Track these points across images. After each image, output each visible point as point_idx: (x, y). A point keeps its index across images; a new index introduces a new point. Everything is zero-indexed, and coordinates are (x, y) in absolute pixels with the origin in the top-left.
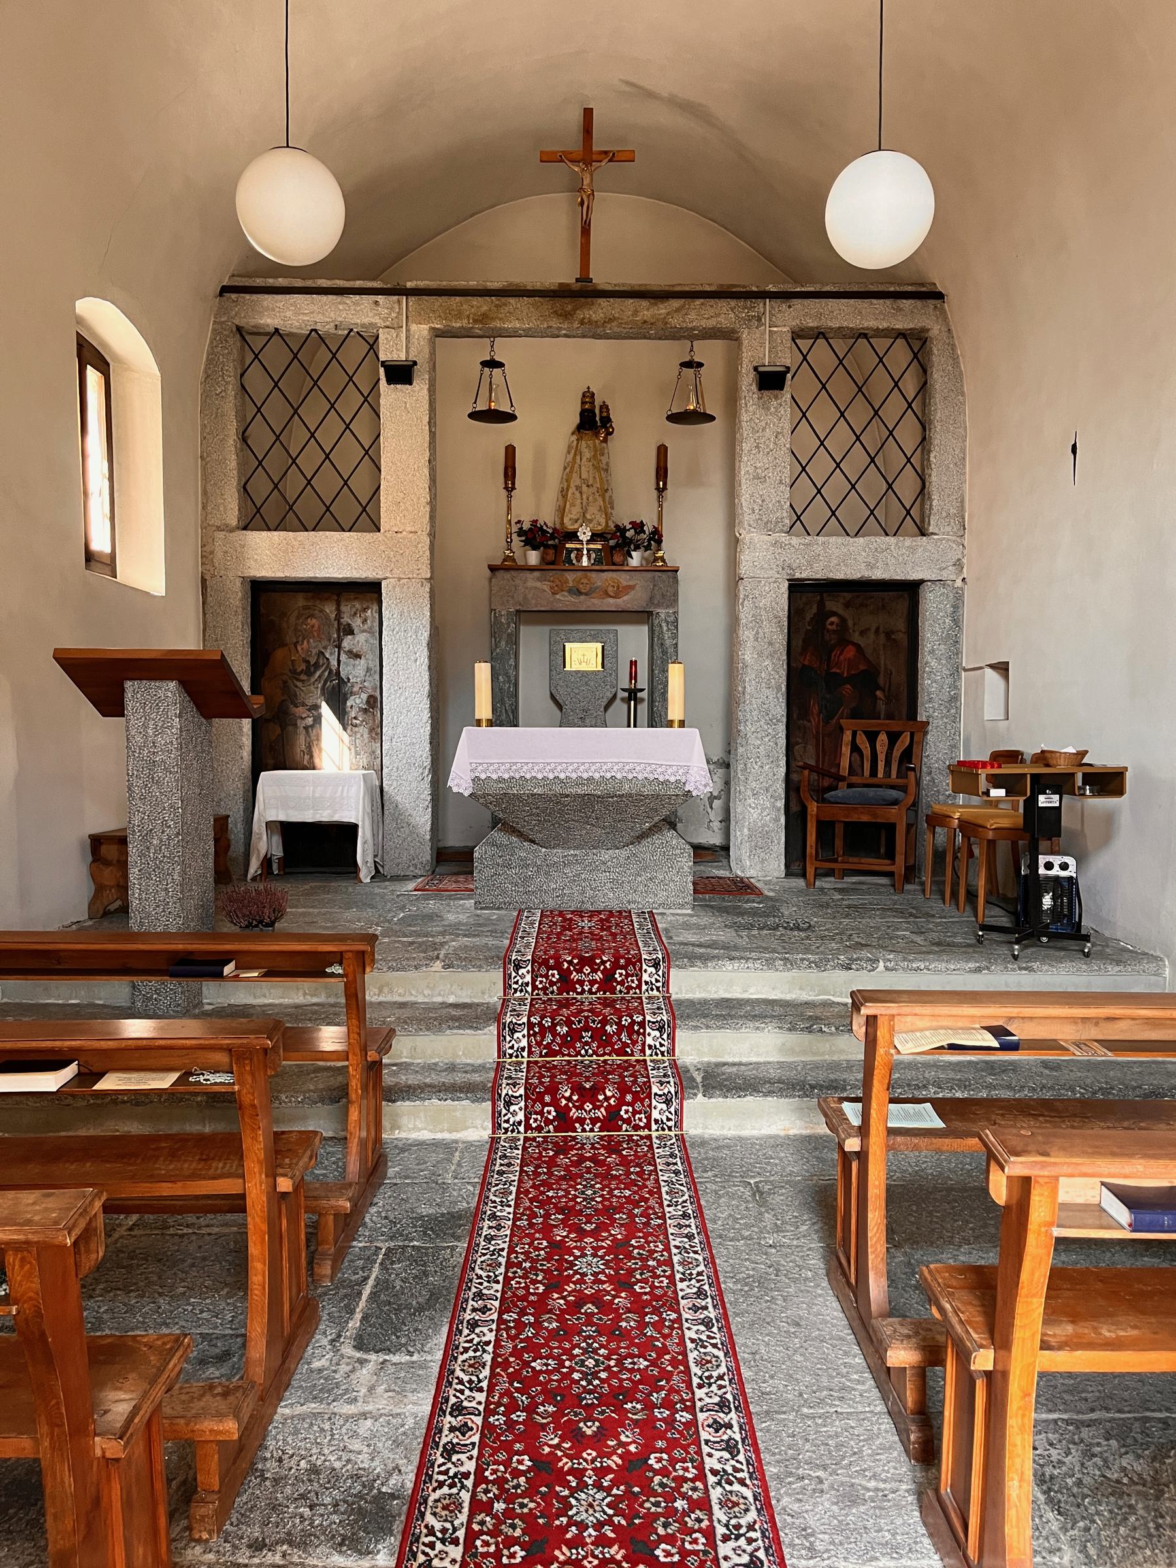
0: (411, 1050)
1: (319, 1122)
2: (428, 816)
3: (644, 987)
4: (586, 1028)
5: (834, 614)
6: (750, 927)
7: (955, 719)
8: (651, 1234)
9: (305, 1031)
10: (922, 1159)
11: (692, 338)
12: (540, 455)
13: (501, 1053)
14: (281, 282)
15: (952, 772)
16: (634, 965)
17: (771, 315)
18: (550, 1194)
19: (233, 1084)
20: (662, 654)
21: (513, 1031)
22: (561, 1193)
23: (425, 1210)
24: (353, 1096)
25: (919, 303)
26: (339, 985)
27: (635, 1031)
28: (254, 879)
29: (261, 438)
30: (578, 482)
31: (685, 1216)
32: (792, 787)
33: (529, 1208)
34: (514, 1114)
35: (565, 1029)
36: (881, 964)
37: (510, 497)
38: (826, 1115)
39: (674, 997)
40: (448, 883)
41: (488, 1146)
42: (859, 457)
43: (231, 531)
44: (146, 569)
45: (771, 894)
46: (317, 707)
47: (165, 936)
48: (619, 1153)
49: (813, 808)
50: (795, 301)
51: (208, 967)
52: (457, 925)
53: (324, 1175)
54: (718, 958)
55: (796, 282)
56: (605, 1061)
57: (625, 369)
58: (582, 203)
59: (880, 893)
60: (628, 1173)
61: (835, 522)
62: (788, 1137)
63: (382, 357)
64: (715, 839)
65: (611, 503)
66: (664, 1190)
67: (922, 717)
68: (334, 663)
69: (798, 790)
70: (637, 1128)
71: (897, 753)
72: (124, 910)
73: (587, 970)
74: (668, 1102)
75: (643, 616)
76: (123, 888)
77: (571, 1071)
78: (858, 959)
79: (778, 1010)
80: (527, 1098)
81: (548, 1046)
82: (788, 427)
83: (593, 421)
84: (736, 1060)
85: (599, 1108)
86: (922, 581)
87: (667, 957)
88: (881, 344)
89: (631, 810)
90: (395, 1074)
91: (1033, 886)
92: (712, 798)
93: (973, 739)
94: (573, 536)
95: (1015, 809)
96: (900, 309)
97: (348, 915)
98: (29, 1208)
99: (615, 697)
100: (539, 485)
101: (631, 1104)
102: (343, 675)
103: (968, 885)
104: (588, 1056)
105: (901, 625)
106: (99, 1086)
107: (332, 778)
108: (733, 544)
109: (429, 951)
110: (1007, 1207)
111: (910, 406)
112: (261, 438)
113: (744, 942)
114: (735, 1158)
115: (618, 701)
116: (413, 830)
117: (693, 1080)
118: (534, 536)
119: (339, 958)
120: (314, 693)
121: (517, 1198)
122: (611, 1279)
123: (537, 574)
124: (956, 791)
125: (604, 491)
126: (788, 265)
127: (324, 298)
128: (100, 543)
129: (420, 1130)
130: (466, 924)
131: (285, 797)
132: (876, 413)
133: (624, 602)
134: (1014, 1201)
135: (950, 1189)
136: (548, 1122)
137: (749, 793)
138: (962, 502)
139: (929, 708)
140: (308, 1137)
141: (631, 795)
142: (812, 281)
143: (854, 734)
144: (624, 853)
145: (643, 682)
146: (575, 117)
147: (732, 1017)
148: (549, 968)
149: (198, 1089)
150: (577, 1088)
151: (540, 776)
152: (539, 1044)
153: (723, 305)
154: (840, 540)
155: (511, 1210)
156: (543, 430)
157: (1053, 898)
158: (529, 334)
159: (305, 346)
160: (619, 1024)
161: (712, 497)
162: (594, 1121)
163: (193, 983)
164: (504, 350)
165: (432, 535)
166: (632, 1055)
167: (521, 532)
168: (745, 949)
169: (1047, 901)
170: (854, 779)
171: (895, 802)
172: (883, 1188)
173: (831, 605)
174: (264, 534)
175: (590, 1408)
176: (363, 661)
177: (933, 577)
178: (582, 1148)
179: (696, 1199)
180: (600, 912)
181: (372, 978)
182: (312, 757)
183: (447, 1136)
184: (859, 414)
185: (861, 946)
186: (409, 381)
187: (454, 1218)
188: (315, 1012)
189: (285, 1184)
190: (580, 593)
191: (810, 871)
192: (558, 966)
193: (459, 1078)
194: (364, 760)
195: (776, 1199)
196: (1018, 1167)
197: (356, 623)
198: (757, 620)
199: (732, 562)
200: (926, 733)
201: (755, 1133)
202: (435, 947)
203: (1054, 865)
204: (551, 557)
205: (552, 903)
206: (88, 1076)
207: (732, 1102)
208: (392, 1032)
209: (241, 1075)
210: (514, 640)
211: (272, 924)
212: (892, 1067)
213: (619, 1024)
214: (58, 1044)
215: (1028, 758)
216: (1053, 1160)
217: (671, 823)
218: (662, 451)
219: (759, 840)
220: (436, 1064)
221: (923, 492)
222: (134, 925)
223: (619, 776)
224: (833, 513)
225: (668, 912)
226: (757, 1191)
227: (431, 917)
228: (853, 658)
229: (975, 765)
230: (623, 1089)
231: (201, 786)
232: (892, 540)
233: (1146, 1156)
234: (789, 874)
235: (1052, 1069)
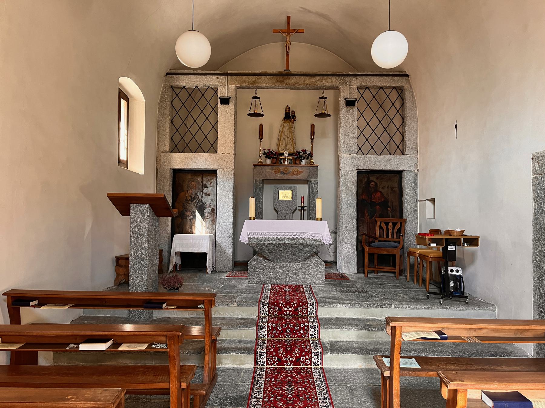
0: (228, 335)
1: (192, 362)
2: (231, 250)
3: (308, 313)
4: (288, 328)
5: (373, 181)
6: (346, 291)
7: (416, 218)
8: (313, 405)
9: (189, 328)
10: (411, 379)
11: (323, 89)
12: (271, 127)
13: (258, 336)
14: (186, 71)
15: (417, 237)
16: (305, 305)
17: (350, 82)
18: (276, 389)
20: (313, 195)
21: (262, 329)
22: (280, 389)
23: (231, 394)
24: (207, 352)
25: (400, 78)
26: (202, 312)
27: (306, 329)
28: (171, 272)
29: (178, 122)
30: (284, 137)
31: (325, 398)
32: (359, 241)
33: (269, 394)
34: (263, 359)
35: (281, 328)
36: (393, 306)
37: (261, 141)
38: (376, 362)
42: (380, 129)
43: (167, 153)
44: (138, 165)
47: (141, 293)
48: (300, 374)
49: (367, 249)
50: (358, 77)
51: (157, 305)
53: (195, 381)
54: (335, 303)
55: (358, 71)
56: (295, 340)
57: (302, 100)
58: (287, 46)
60: (304, 382)
61: (373, 150)
63: (219, 96)
64: (331, 259)
65: (295, 144)
66: (317, 388)
67: (404, 217)
69: (361, 242)
70: (306, 365)
71: (396, 230)
72: (127, 283)
73: (288, 307)
74: (318, 356)
75: (306, 181)
76: (127, 275)
77: (283, 344)
78: (385, 304)
79: (357, 322)
80: (267, 353)
81: (274, 334)
82: (356, 119)
83: (289, 116)
84: (342, 340)
85: (293, 357)
86: (403, 171)
87: (317, 302)
88: (388, 91)
89: (303, 249)
90: (220, 343)
91: (446, 278)
92: (330, 244)
93: (423, 226)
94: (282, 154)
95: (439, 249)
96: (394, 80)
97: (204, 285)
98: (100, 395)
99: (296, 209)
100: (271, 137)
101: (304, 356)
102: (203, 201)
103: (422, 277)
104: (289, 338)
105: (396, 185)
107: (199, 236)
109: (232, 299)
110: (448, 400)
111: (398, 111)
112: (178, 122)
113: (344, 297)
114: (342, 376)
115: (297, 211)
116: (226, 254)
117: (327, 347)
118: (269, 154)
119: (203, 302)
121: (264, 390)
123: (270, 167)
124: (418, 244)
125: (293, 140)
126: (354, 64)
127: (200, 76)
128: (123, 157)
129: (229, 364)
130: (245, 289)
131: (183, 243)
132: (386, 114)
133: (300, 177)
134: (451, 398)
135: (421, 390)
136: (275, 362)
137: (344, 243)
138: (417, 143)
140: (191, 368)
141: (303, 244)
142: (364, 71)
143: (381, 223)
144: (301, 264)
145: (306, 204)
146: (285, 19)
147: (340, 324)
148: (275, 306)
149: (155, 350)
151: (271, 237)
152: (271, 333)
153: (334, 78)
154: (375, 156)
155: (262, 395)
156: (273, 120)
157: (454, 283)
158: (268, 88)
159: (192, 92)
160: (300, 326)
161: (329, 142)
162: (291, 362)
163: (150, 310)
165: (235, 154)
167: (264, 153)
168: (344, 300)
169: (452, 283)
170: (381, 239)
171: (396, 247)
172: (399, 390)
173: (372, 178)
174: (178, 154)
176: (210, 197)
178: (287, 372)
179: (328, 392)
180: (292, 285)
182: (192, 229)
183: (238, 366)
184: (380, 114)
187: (242, 397)
188: (192, 321)
189: (184, 385)
190: (285, 174)
191: (366, 271)
192: (278, 305)
193: (243, 345)
196: (452, 386)
197: (208, 184)
198: (346, 184)
199: (337, 163)
200: (406, 223)
201: (349, 367)
202: (235, 297)
203: (454, 271)
204: (274, 161)
205: (275, 282)
206: (116, 345)
207: (341, 356)
208: (220, 329)
209: (170, 345)
210: (262, 190)
211: (178, 289)
213: (300, 326)
214: (107, 333)
217: (316, 254)
218: (313, 126)
219: (348, 261)
220: (234, 340)
221: (403, 140)
222: (131, 289)
223: (299, 237)
224: (372, 147)
225: (316, 285)
226: (351, 389)
227: (232, 287)
228: (380, 197)
229: (424, 235)
230: (302, 350)
231: (155, 240)
232: (392, 156)
233: (498, 381)
234: (358, 272)
235: (456, 345)
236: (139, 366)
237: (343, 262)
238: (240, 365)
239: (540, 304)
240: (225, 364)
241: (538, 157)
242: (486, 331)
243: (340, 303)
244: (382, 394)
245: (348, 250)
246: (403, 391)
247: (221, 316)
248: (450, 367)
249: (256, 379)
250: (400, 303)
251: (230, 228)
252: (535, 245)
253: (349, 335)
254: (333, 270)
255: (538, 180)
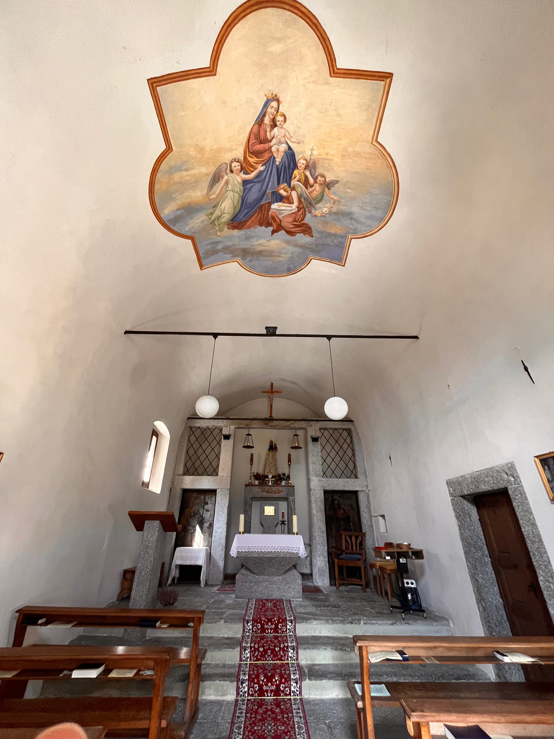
0: (215, 658)
1: (176, 692)
3: (288, 631)
4: (269, 649)
6: (320, 606)
7: (373, 532)
11: (296, 429)
13: (241, 660)
18: (255, 728)
19: (154, 675)
20: (291, 511)
22: (259, 728)
24: (191, 680)
26: (191, 630)
27: (285, 650)
29: (191, 452)
32: (329, 554)
39: (298, 635)
40: (227, 588)
41: (234, 703)
44: (156, 487)
45: (326, 593)
46: (195, 527)
47: (140, 610)
49: (336, 561)
52: (229, 605)
53: (176, 718)
57: (282, 437)
59: (358, 592)
61: (334, 475)
62: (338, 699)
64: (307, 571)
66: (296, 726)
67: (364, 531)
68: (202, 513)
71: (358, 543)
72: (129, 597)
73: (270, 624)
74: (297, 683)
75: (286, 499)
76: (130, 589)
77: (263, 667)
78: (355, 619)
81: (256, 657)
82: (320, 451)
83: (273, 448)
91: (405, 591)
92: (306, 557)
93: (379, 539)
94: (267, 477)
99: (278, 523)
101: (284, 683)
105: (354, 503)
106: (110, 676)
108: (309, 480)
109: (219, 616)
110: (414, 737)
112: (191, 452)
113: (318, 612)
116: (218, 567)
118: (257, 477)
119: (192, 620)
120: (195, 521)
122: (275, 704)
125: (275, 465)
133: (281, 495)
139: (365, 529)
141: (283, 557)
142: (323, 417)
144: (281, 577)
146: (269, 384)
148: (258, 623)
150: (266, 676)
156: (261, 450)
157: (411, 595)
158: (258, 428)
161: (303, 466)
163: (143, 629)
164: (252, 432)
165: (231, 477)
166: (284, 661)
167: (254, 476)
170: (347, 551)
171: (359, 560)
173: (335, 497)
175: (269, 717)
177: (361, 489)
178: (267, 705)
180: (273, 600)
181: (203, 627)
183: (219, 698)
184: (337, 447)
185: (355, 614)
186: (229, 439)
190: (269, 492)
191: (337, 583)
194: (206, 543)
195: (336, 731)
197: (209, 501)
198: (316, 501)
200: (365, 536)
202: (223, 613)
205: (259, 596)
206: (107, 671)
208: (206, 651)
210: (251, 506)
211: (172, 604)
212: (371, 665)
213: (280, 647)
214: (101, 657)
215: (395, 545)
216: (426, 714)
217: (295, 566)
218: (289, 455)
220: (219, 664)
221: (355, 467)
225: (295, 600)
227: (222, 601)
228: (343, 514)
230: (281, 676)
234: (331, 585)
236: (124, 698)
237: (317, 574)
238: (222, 696)
239: (486, 618)
240: (208, 695)
241: (450, 483)
242: (442, 648)
243: (315, 619)
244: (359, 733)
245: (321, 562)
246: (376, 727)
247: (208, 635)
248: (417, 694)
249: (237, 715)
250: (368, 618)
251: (223, 541)
252: (467, 558)
253: (324, 657)
254: (309, 582)
255: (454, 501)
